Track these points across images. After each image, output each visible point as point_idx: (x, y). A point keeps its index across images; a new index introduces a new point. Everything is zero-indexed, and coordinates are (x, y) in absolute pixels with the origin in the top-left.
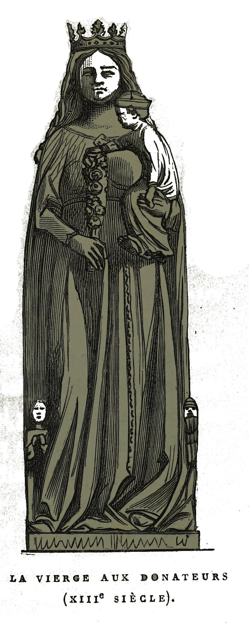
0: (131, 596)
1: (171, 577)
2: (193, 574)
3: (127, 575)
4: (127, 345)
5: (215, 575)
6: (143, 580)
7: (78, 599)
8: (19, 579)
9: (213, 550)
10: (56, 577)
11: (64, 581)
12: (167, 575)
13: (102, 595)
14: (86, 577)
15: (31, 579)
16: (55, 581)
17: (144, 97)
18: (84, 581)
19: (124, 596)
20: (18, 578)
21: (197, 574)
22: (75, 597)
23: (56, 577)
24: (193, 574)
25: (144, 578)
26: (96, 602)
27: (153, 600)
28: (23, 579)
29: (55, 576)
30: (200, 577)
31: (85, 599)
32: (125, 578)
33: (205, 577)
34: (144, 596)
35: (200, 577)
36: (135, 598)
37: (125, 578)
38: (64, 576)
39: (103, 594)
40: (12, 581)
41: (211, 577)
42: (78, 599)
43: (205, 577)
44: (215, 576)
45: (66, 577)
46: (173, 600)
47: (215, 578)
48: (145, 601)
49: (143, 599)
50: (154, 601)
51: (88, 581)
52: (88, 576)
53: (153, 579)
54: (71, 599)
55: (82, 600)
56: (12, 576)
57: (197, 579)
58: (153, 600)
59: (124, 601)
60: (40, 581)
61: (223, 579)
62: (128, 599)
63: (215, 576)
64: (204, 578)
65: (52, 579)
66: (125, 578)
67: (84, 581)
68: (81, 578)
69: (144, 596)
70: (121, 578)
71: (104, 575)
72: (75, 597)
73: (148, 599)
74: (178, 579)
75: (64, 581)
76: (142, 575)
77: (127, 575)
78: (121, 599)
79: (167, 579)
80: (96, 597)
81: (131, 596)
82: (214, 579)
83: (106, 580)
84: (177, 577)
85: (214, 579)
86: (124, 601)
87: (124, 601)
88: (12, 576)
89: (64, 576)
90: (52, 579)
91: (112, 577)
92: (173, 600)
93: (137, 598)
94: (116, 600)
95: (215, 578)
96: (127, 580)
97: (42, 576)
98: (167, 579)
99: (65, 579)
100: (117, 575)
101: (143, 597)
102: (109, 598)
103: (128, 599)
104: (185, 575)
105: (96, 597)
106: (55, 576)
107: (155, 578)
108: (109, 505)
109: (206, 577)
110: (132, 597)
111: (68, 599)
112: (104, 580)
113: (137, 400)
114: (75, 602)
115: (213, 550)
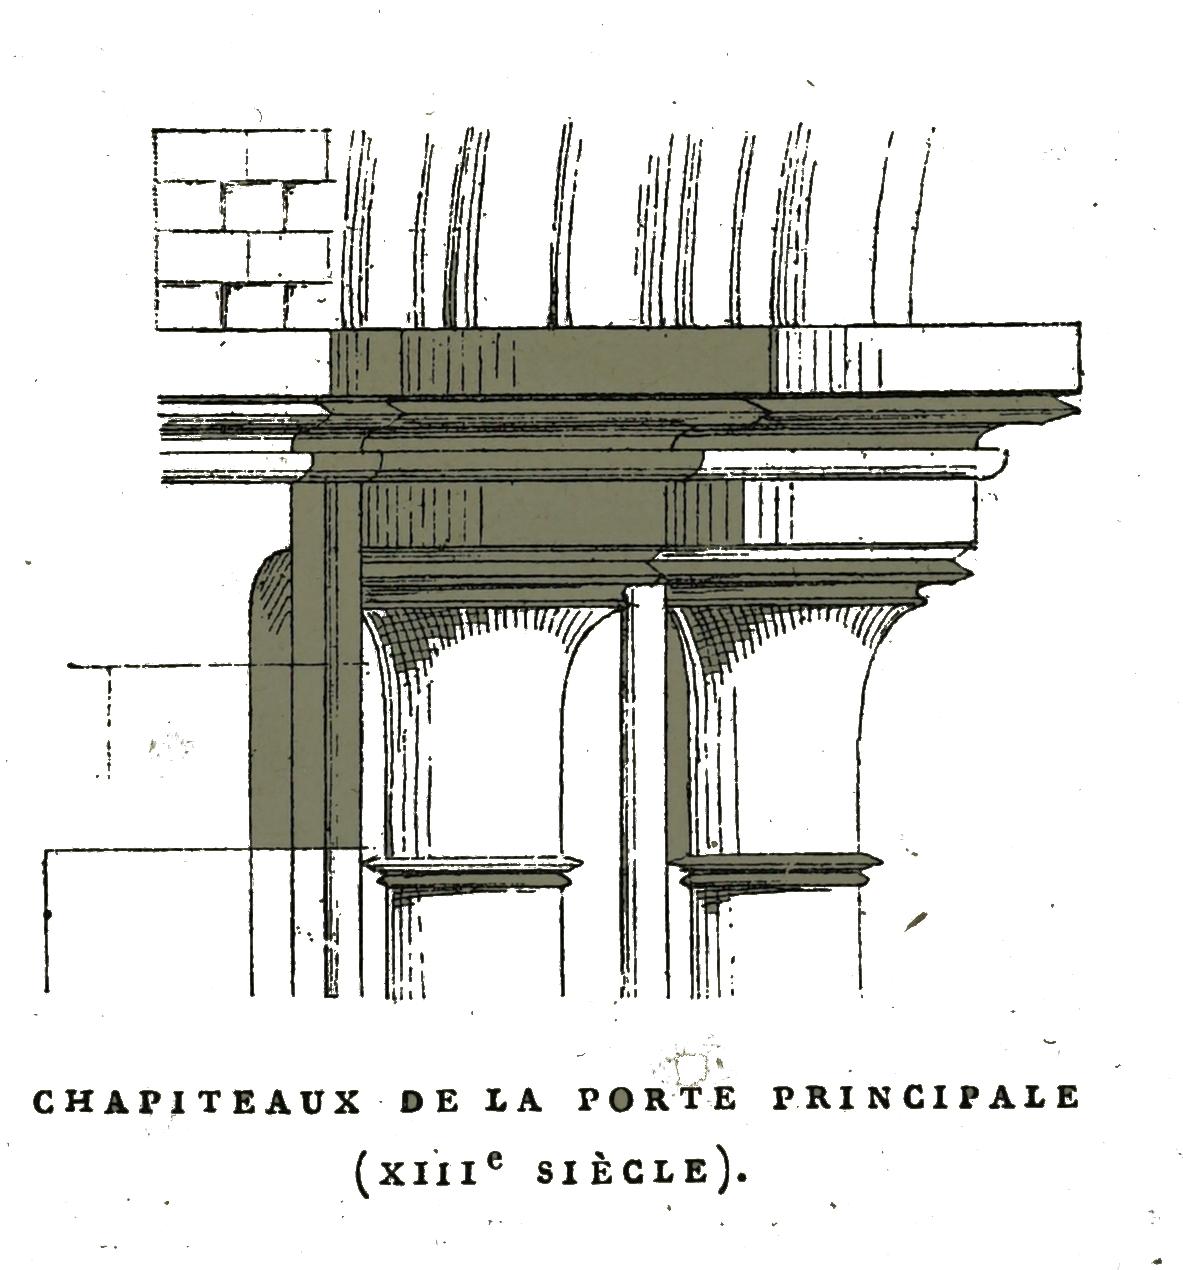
1: (261, 1101)
3: (353, 1093)
4: (222, 313)
6: (405, 1109)
7: (408, 1173)
9: (293, 994)
10: (969, 1094)
11: (650, 1107)
13: (494, 1158)
14: (1065, 1092)
19: (570, 1165)
20: (512, 1096)
21: (453, 1092)
22: (398, 1165)
23: (243, 1098)
24: (441, 1093)
26: (468, 1181)
27: (666, 1175)
29: (238, 1094)
31: (432, 1174)
32: (347, 1104)
34: (919, 1088)
37: (347, 1103)
38: (811, 1089)
39: (499, 1157)
40: (493, 1107)
42: (408, 1173)
44: (817, 1095)
46: (742, 1178)
47: (817, 1101)
48: (639, 1179)
49: (634, 1172)
50: (1041, 1104)
51: (732, 1106)
52: (251, 1093)
53: (617, 1110)
56: (494, 1093)
57: (455, 1108)
58: (666, 1175)
59: (570, 1180)
61: (919, 1088)
63: (817, 1095)
65: (860, 1097)
66: (347, 1104)
68: (431, 1101)
69: (49, 1094)
70: (331, 1102)
72: (398, 1165)
73: (650, 1171)
74: (1009, 1105)
77: (353, 1093)
78: (559, 1172)
81: (596, 1164)
84: (532, 1101)
86: (570, 1180)
88: (494, 1093)
89: (811, 1089)
90: (860, 1097)
94: (545, 1173)
95: (817, 1101)
96: (354, 1110)
100: (319, 1094)
101: (44, 1097)
102: (520, 1167)
104: (210, 1094)
106: (1062, 1088)
108: (387, 859)
109: (313, 1105)
111: (373, 1173)
112: (277, 1109)
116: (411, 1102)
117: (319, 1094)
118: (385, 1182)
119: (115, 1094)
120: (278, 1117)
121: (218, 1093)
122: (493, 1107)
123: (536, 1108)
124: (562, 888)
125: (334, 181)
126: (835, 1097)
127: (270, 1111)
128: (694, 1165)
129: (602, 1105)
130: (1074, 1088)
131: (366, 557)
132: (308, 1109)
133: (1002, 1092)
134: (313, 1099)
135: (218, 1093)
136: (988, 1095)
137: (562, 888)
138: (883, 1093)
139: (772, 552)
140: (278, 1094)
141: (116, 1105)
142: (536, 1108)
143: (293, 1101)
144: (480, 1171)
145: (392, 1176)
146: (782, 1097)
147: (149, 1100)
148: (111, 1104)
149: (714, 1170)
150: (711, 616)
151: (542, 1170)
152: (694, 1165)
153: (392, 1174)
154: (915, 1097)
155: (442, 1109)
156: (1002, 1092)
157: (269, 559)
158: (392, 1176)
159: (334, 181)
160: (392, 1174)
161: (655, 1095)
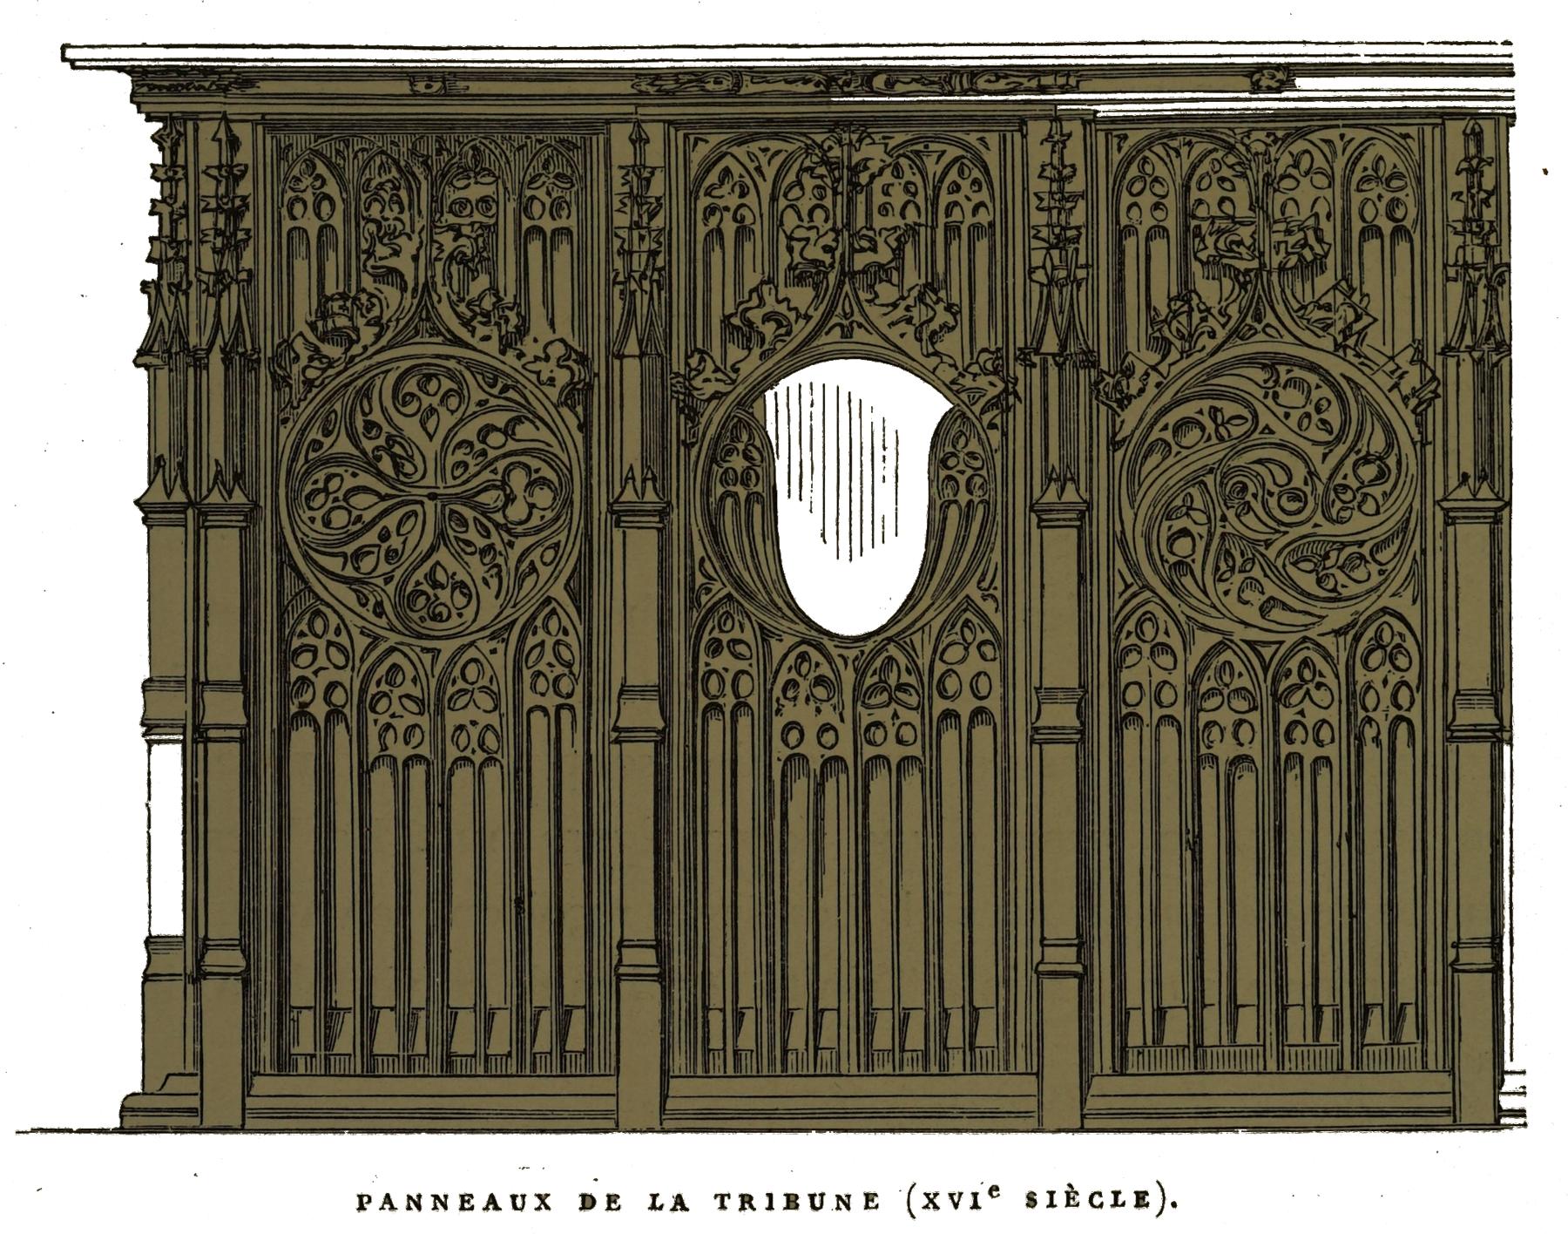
1: (480, 1201)
8: (670, 1203)
11: (742, 1208)
12: (848, 1196)
13: (993, 1190)
15: (634, 1203)
20: (667, 1200)
22: (936, 1195)
25: (588, 1203)
26: (975, 1206)
28: (680, 1203)
30: (804, 1202)
33: (792, 1202)
35: (804, 1202)
38: (742, 1196)
39: (997, 1189)
40: (653, 1207)
41: (830, 1202)
43: (519, 1202)
46: (1174, 1205)
52: (1146, 1193)
55: (1116, 1199)
56: (654, 1196)
60: (956, 1206)
61: (1100, 1194)
62: (1060, 1199)
64: (515, 1207)
68: (602, 1202)
69: (1100, 1194)
71: (388, 1196)
73: (1108, 1199)
74: (497, 1208)
76: (584, 1196)
78: (1043, 1199)
79: (848, 1207)
80: (975, 1195)
81: (1068, 1193)
86: (1051, 1205)
87: (1051, 1205)
88: (654, 1196)
89: (742, 1196)
90: (780, 1202)
92: (1174, 1205)
93: (1083, 1198)
94: (1031, 1201)
96: (927, 1195)
100: (822, 1195)
103: (1060, 1199)
104: (723, 1196)
109: (519, 1204)
111: (919, 1200)
114: (539, 1196)
116: (587, 1202)
117: (822, 1195)
118: (926, 1207)
120: (491, 1212)
122: (653, 1207)
123: (684, 1209)
124: (150, 936)
126: (760, 1202)
127: (486, 1209)
129: (372, 1208)
132: (813, 1207)
133: (492, 1200)
136: (378, 1200)
137: (150, 936)
139: (1376, 79)
141: (1141, 1199)
142: (684, 1209)
143: (504, 1201)
144: (984, 1199)
147: (465, 1201)
150: (640, 216)
153: (931, 1201)
155: (609, 1208)
156: (492, 1200)
157: (936, 433)
158: (931, 1201)
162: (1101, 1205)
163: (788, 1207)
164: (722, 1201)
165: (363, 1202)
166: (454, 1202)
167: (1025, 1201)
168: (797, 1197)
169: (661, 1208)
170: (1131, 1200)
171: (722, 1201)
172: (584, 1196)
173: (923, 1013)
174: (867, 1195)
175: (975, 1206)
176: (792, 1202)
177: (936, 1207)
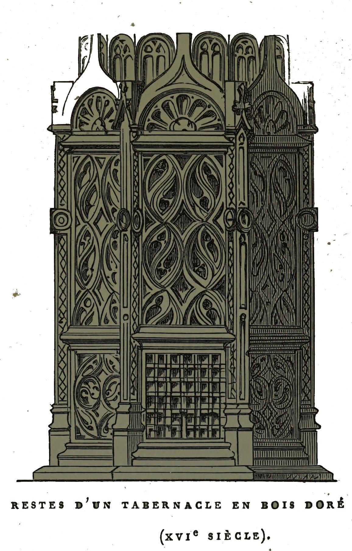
0: (226, 534)
1: (183, 505)
2: (23, 502)
5: (15, 504)
9: (18, 481)
10: (227, 535)
11: (328, 507)
16: (339, 507)
17: (54, 134)
18: (154, 508)
22: (171, 534)
26: (188, 539)
33: (146, 505)
34: (200, 503)
35: (151, 505)
36: (230, 536)
38: (163, 502)
45: (330, 504)
48: (201, 507)
49: (238, 536)
50: (40, 503)
51: (343, 507)
54: (166, 537)
60: (179, 539)
61: (200, 503)
62: (222, 536)
67: (154, 508)
69: (240, 533)
71: (135, 503)
72: (171, 534)
73: (204, 505)
75: (328, 507)
78: (215, 536)
80: (188, 535)
81: (226, 534)
82: (13, 508)
83: (137, 508)
85: (13, 508)
86: (219, 539)
89: (163, 502)
91: (283, 504)
93: (232, 536)
97: (181, 534)
98: (109, 507)
99: (163, 505)
103: (222, 536)
104: (42, 503)
105: (188, 535)
107: (275, 506)
109: (96, 506)
110: (227, 535)
111: (164, 537)
113: (245, 282)
115: (18, 481)
119: (188, 503)
121: (45, 503)
125: (336, 481)
128: (255, 534)
130: (54, 502)
131: (106, 458)
134: (96, 505)
135: (45, 503)
138: (106, 506)
140: (135, 503)
141: (188, 506)
143: (193, 505)
144: (191, 536)
145: (169, 538)
146: (107, 505)
148: (187, 506)
149: (261, 535)
151: (209, 536)
152: (255, 534)
153: (169, 537)
154: (199, 505)
159: (336, 481)
160: (169, 537)
161: (165, 504)
162: (240, 538)
163: (144, 508)
164: (125, 505)
165: (14, 505)
166: (241, 505)
167: (17, 296)
168: (148, 503)
169: (210, 507)
170: (214, 506)
171: (125, 505)
172: (77, 503)
173: (111, 478)
174: (234, 503)
175: (188, 539)
176: (146, 505)
177: (171, 540)
